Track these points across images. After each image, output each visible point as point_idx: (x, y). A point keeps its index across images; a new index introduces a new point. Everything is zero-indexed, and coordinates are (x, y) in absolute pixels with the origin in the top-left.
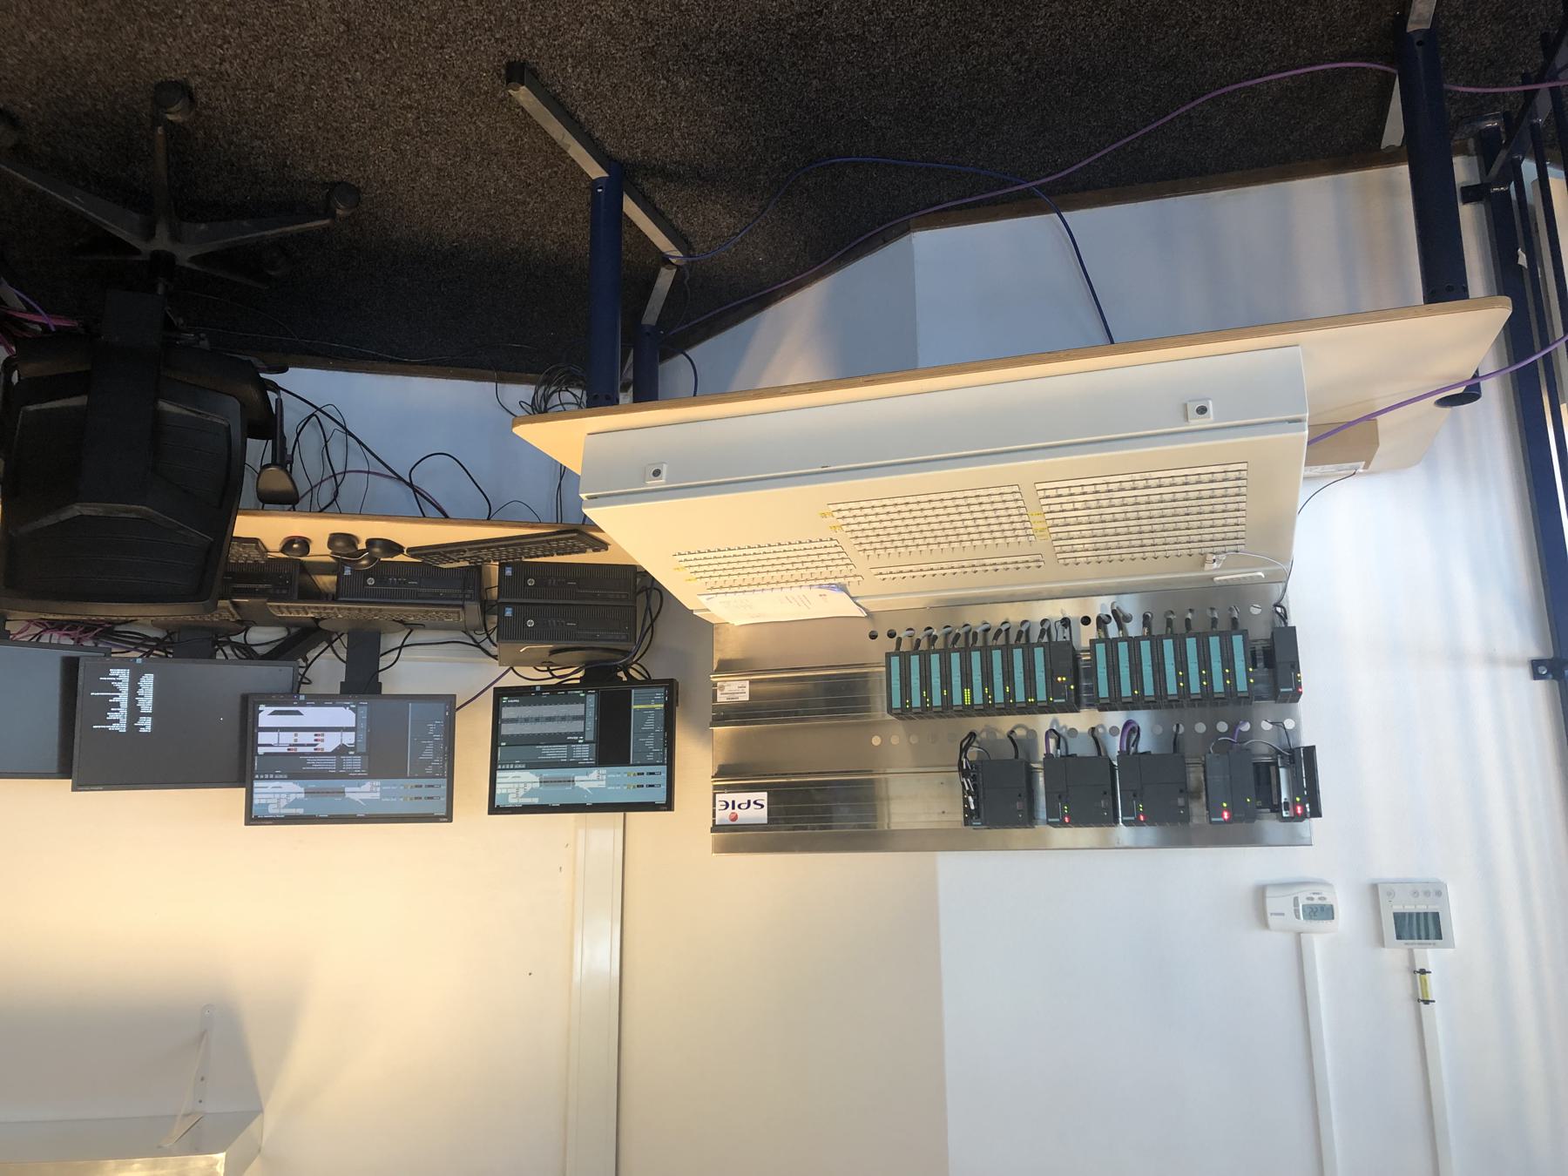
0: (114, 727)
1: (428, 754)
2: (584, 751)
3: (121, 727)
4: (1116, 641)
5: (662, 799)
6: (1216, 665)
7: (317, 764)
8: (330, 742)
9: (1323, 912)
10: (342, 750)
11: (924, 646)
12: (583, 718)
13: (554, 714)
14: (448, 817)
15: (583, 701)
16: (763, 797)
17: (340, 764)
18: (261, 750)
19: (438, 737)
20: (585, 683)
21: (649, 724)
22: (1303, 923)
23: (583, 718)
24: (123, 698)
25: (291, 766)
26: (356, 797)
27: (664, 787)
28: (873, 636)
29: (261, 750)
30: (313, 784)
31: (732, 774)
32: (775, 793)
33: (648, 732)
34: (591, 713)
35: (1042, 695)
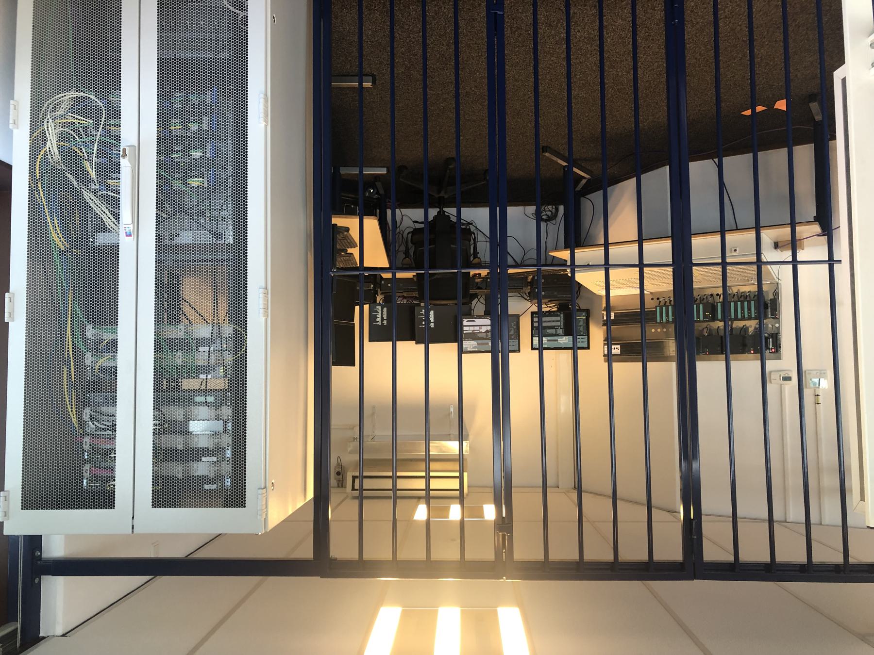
0: (378, 323)
1: (512, 332)
2: (560, 331)
3: (379, 323)
4: (668, 306)
5: (586, 346)
6: (746, 310)
7: (480, 336)
8: (484, 329)
9: (788, 379)
10: (487, 332)
11: (668, 303)
12: (560, 321)
13: (550, 320)
14: (519, 351)
15: (559, 316)
16: (619, 347)
17: (556, 332)
18: (465, 332)
19: (515, 327)
20: (559, 310)
21: (581, 323)
22: (782, 382)
23: (560, 321)
24: (379, 316)
25: (473, 336)
26: (561, 342)
27: (586, 342)
28: (652, 299)
29: (465, 332)
30: (480, 342)
31: (609, 341)
32: (622, 346)
33: (581, 326)
34: (562, 320)
35: (701, 318)
